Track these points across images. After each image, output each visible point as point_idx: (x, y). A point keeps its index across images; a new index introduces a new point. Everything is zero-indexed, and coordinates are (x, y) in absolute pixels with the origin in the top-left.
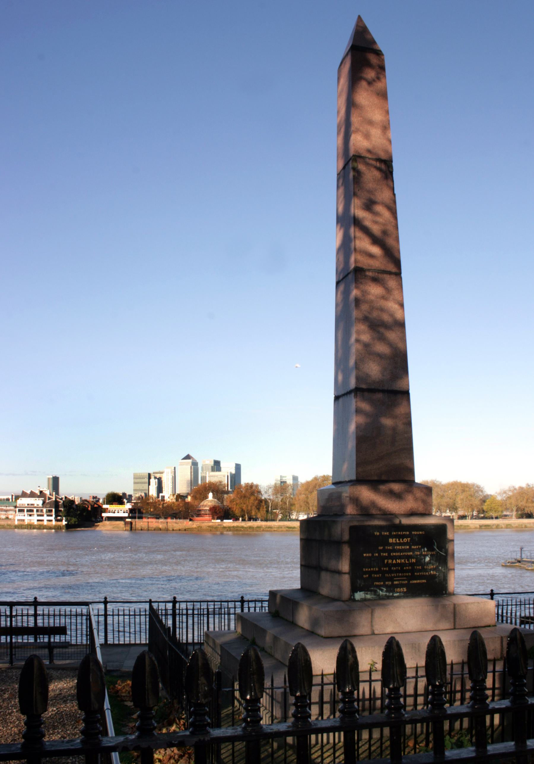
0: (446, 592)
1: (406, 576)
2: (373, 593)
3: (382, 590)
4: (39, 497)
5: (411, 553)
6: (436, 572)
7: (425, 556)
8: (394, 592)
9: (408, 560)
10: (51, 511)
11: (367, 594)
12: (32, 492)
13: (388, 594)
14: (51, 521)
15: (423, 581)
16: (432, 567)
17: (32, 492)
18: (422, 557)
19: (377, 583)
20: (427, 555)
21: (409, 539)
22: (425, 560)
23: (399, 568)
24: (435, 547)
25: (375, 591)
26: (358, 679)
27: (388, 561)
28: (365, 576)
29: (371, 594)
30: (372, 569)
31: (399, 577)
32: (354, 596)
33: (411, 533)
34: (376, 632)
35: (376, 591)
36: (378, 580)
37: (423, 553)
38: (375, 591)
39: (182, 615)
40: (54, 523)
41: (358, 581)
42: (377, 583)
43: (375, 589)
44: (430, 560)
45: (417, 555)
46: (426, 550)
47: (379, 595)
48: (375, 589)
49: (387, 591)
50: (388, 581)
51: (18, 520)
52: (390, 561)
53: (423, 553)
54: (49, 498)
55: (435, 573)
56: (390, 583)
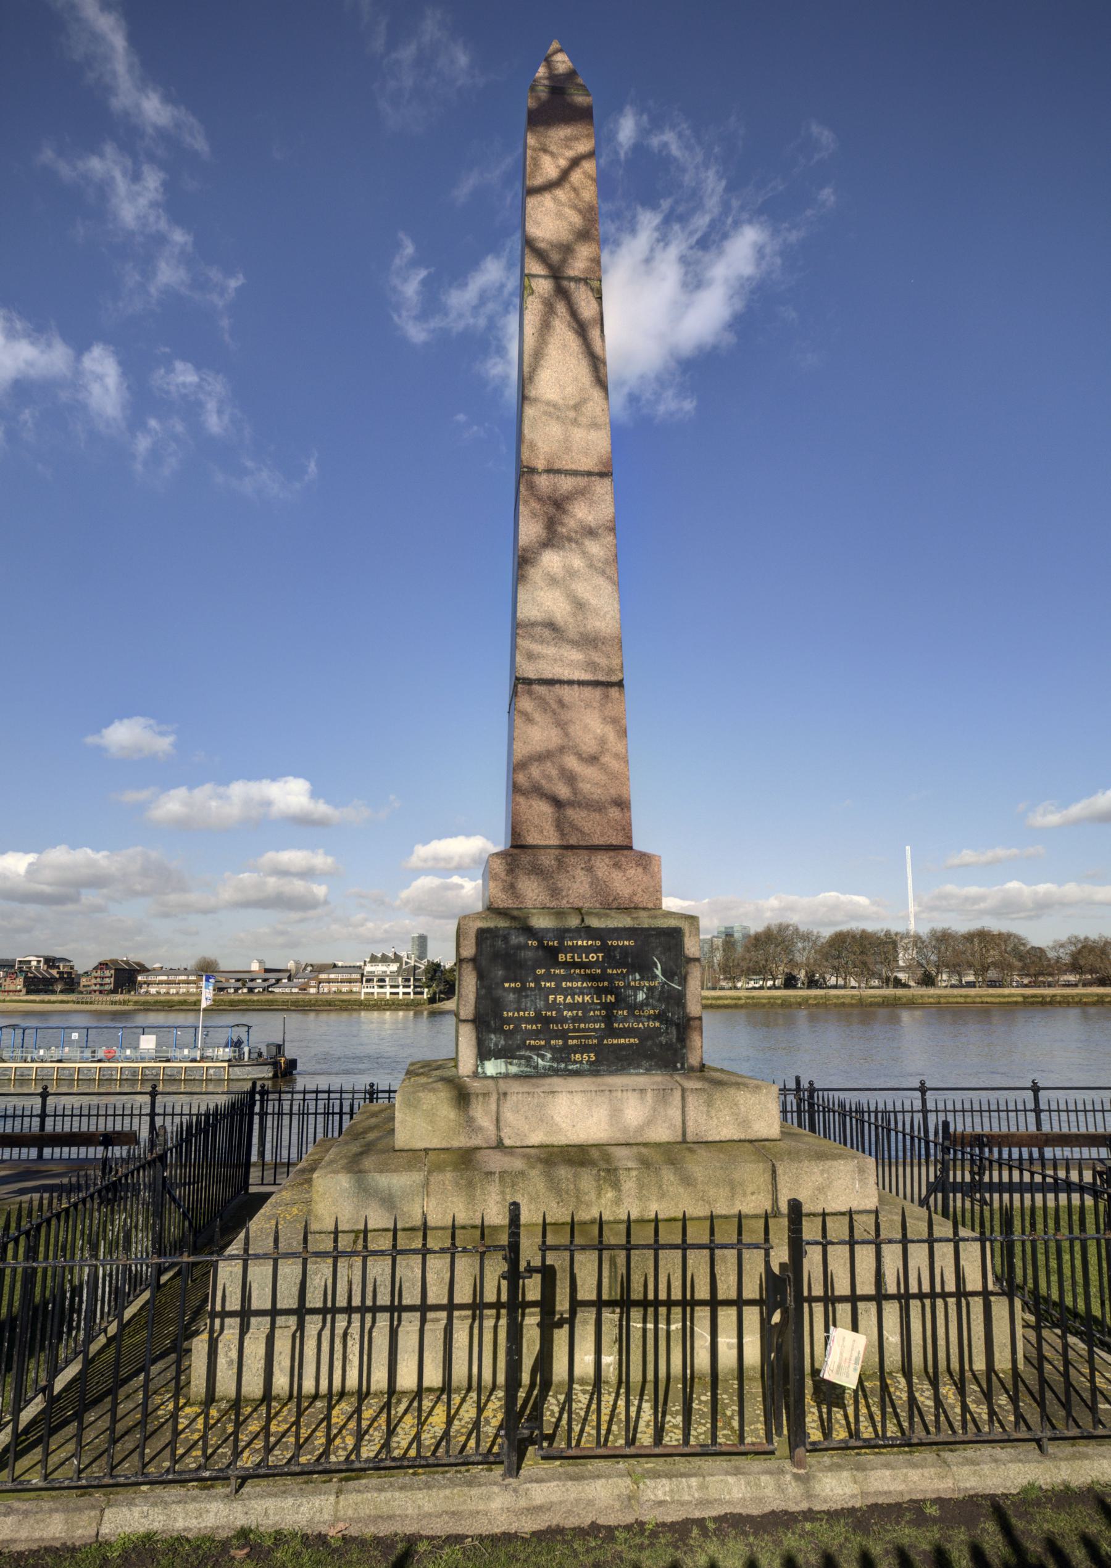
0: (683, 1065)
1: (594, 1030)
2: (523, 1061)
3: (543, 1057)
4: (393, 961)
5: (606, 984)
6: (661, 1024)
7: (637, 989)
8: (567, 1060)
9: (599, 998)
10: (409, 980)
11: (511, 1064)
12: (384, 955)
13: (555, 1065)
14: (409, 993)
15: (632, 1040)
16: (652, 1012)
17: (384, 955)
18: (630, 992)
19: (532, 1042)
20: (640, 988)
21: (600, 955)
22: (636, 999)
23: (580, 1013)
24: (658, 972)
25: (528, 1059)
26: (801, 1210)
27: (555, 999)
28: (506, 1028)
29: (519, 1065)
30: (521, 1013)
31: (579, 1030)
32: (483, 1068)
33: (604, 943)
34: (507, 1142)
35: (531, 1057)
36: (536, 1034)
37: (632, 983)
38: (528, 1059)
39: (308, 1114)
40: (412, 996)
41: (493, 1036)
42: (532, 1042)
43: (528, 1053)
44: (647, 998)
45: (619, 987)
46: (638, 977)
47: (536, 1067)
48: (528, 1053)
49: (553, 1059)
50: (557, 1038)
51: (366, 994)
52: (560, 999)
53: (632, 983)
54: (407, 963)
55: (657, 1024)
56: (560, 1042)
